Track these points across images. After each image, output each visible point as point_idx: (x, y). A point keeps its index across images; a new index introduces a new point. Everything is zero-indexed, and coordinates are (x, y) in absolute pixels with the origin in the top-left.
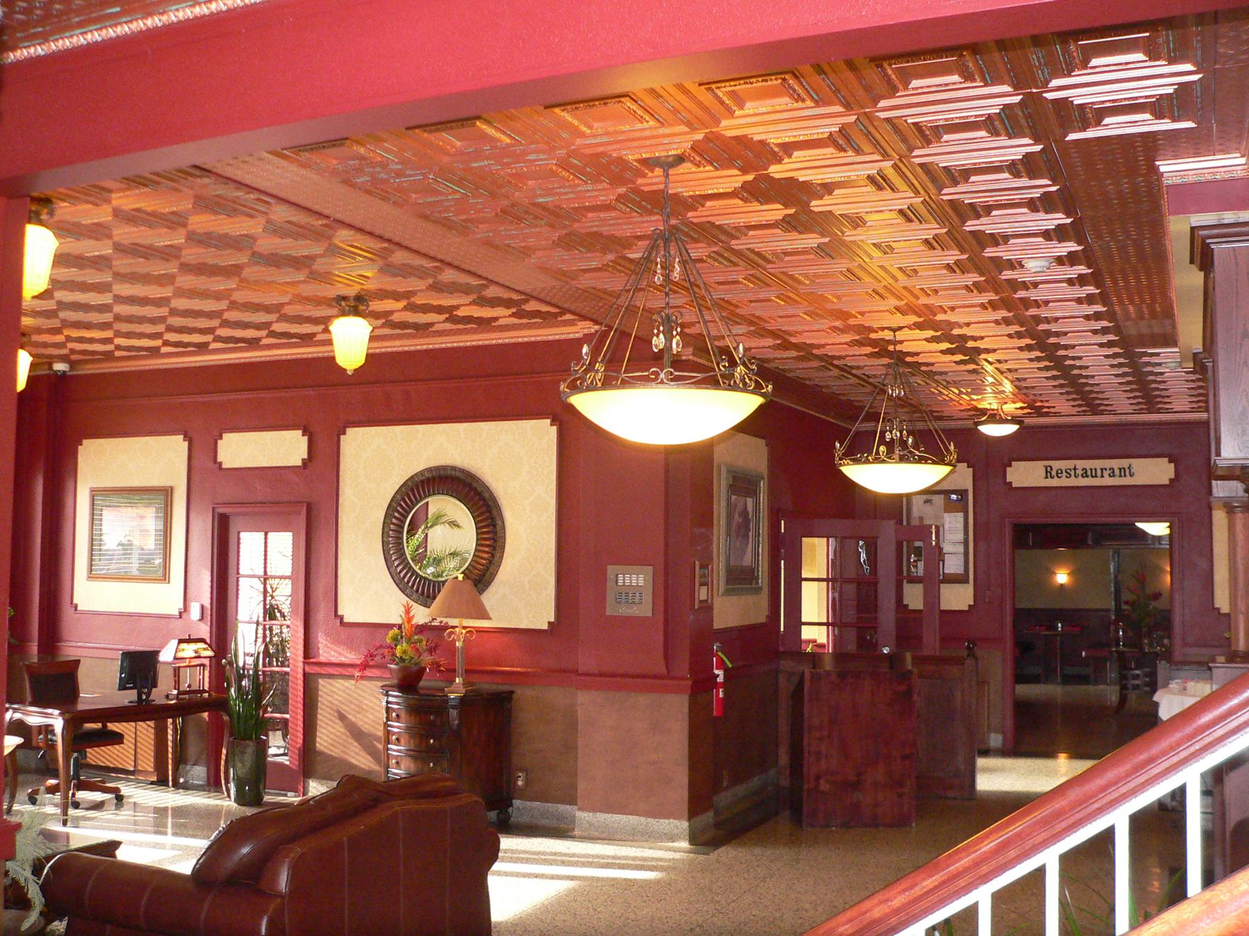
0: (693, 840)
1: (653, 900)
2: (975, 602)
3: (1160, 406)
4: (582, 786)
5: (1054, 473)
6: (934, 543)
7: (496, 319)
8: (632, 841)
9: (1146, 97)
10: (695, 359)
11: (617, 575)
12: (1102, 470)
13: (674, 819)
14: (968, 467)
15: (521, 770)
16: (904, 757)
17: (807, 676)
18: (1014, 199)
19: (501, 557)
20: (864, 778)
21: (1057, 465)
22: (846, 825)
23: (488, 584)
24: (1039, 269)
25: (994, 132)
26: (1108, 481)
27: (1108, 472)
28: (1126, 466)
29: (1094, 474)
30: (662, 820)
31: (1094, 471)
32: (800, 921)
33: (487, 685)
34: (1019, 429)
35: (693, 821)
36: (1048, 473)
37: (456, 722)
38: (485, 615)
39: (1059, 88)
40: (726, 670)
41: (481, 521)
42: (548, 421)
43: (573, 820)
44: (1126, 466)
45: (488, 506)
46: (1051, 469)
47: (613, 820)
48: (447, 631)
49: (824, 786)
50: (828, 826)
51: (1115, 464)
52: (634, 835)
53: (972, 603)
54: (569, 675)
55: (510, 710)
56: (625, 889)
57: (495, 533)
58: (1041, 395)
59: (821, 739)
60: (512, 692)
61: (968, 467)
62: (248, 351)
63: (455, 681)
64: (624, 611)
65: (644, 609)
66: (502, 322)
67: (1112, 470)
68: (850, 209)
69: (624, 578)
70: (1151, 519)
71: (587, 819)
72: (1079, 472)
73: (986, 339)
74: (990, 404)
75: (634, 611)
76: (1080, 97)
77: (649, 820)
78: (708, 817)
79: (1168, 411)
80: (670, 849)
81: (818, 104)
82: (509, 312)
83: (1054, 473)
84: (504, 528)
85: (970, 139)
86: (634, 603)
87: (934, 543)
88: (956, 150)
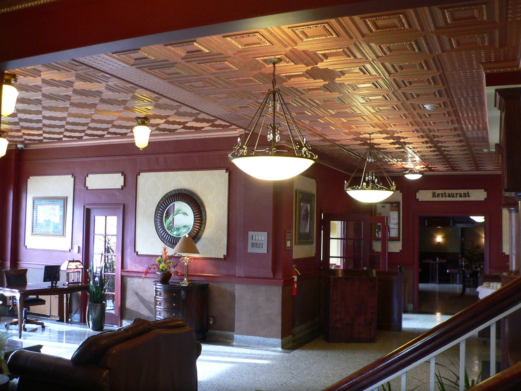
0: (284, 347)
5: (436, 195)
7: (203, 127)
11: (252, 236)
13: (275, 338)
15: (212, 317)
19: (204, 228)
21: (437, 192)
23: (199, 238)
26: (459, 199)
27: (459, 195)
29: (453, 196)
30: (270, 339)
31: (453, 195)
36: (434, 195)
40: (298, 277)
42: (225, 171)
46: (435, 194)
51: (462, 191)
54: (231, 277)
56: (254, 368)
63: (184, 279)
71: (239, 338)
72: (447, 195)
74: (410, 166)
77: (265, 338)
82: (209, 124)
83: (436, 195)
86: (259, 247)
87: (386, 224)
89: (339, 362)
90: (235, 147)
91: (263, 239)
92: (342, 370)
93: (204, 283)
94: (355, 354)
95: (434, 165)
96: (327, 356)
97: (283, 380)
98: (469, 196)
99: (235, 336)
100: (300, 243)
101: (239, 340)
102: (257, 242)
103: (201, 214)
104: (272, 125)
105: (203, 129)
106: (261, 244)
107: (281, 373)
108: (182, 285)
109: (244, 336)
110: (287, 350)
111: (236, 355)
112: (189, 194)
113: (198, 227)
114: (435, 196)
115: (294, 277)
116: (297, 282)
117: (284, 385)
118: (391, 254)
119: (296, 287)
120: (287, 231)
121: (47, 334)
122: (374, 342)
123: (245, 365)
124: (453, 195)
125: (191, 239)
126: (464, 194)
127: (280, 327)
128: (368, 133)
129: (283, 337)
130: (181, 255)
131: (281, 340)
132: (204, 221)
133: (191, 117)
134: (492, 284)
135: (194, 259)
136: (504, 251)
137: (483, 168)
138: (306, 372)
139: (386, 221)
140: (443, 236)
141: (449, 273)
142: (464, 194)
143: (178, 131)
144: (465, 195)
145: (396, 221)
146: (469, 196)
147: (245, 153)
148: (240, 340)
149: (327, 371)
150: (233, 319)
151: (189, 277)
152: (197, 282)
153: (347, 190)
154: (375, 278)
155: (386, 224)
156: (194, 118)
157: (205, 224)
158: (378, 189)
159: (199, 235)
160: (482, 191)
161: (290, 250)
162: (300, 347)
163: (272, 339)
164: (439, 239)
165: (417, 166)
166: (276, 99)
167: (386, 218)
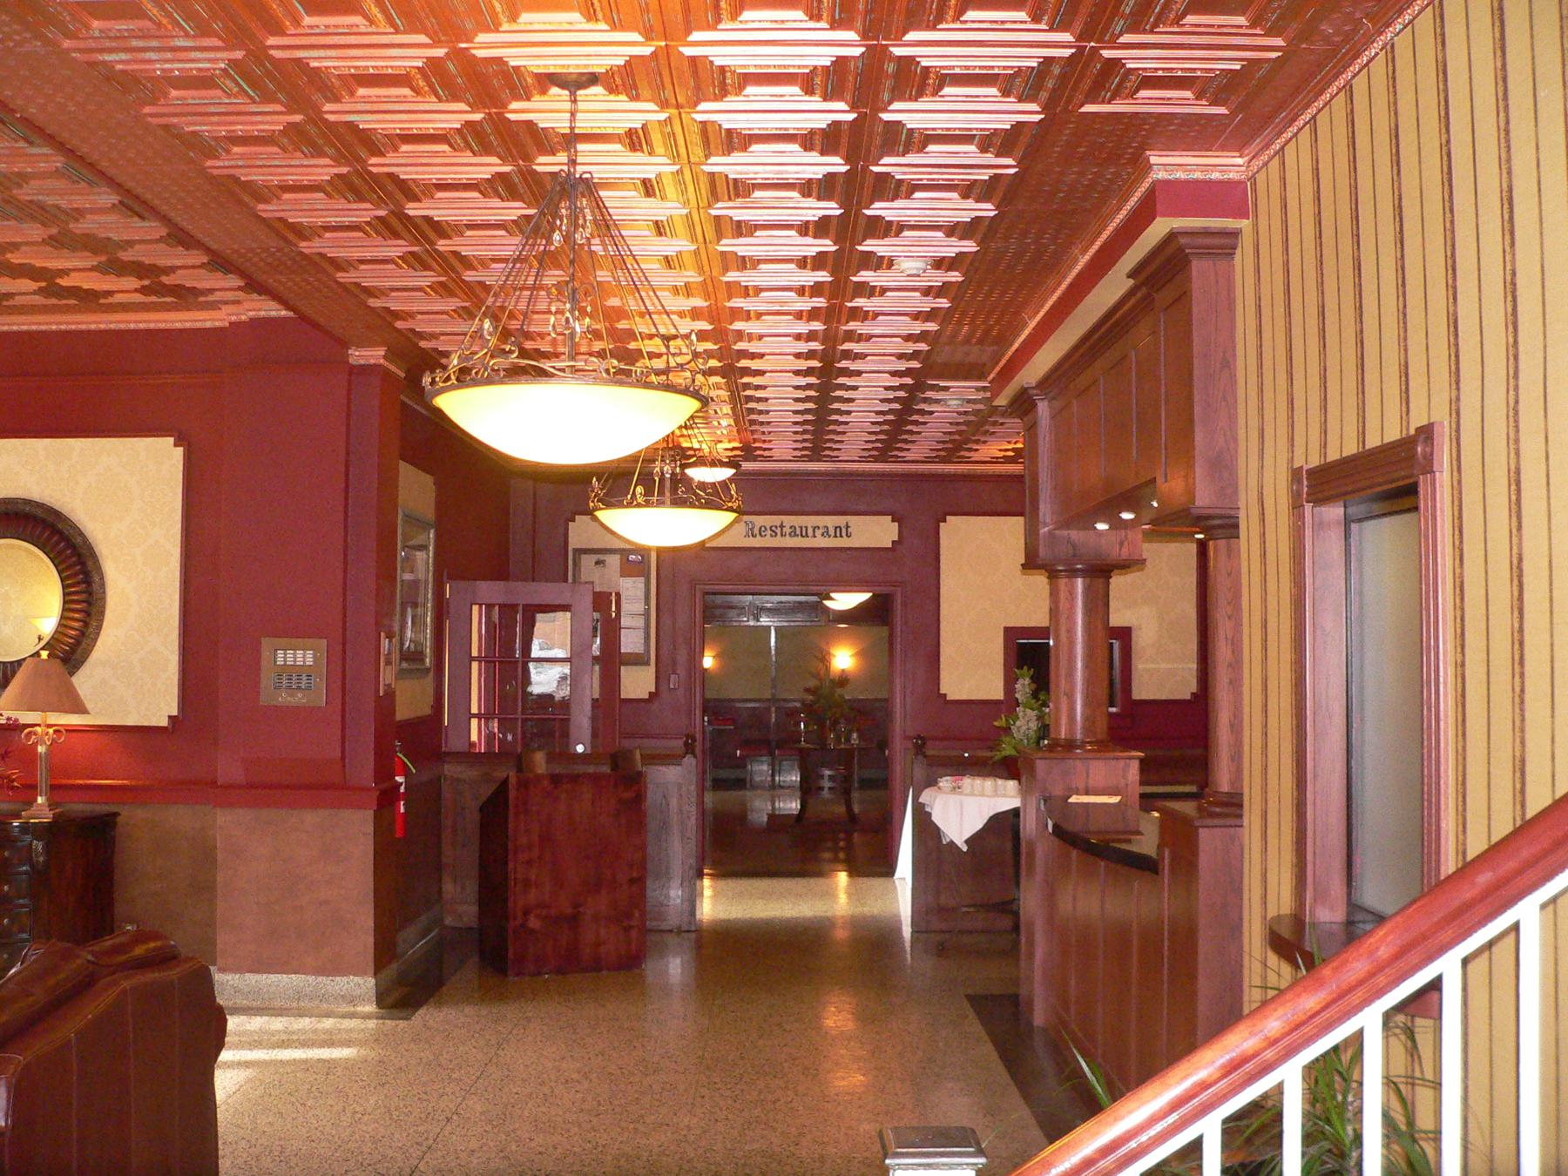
0: (381, 1000)
2: (656, 688)
3: (758, 452)
5: (756, 531)
6: (614, 614)
7: (110, 293)
9: (799, 67)
10: (386, 364)
13: (355, 975)
14: (893, 521)
16: (632, 881)
17: (513, 781)
18: (953, 180)
19: (99, 627)
20: (581, 909)
22: (560, 971)
24: (915, 272)
25: (809, 90)
27: (821, 531)
28: (843, 525)
29: (804, 534)
30: (338, 978)
31: (804, 530)
32: (579, 1096)
33: (79, 807)
34: (734, 475)
35: (379, 975)
37: (41, 859)
38: (80, 709)
39: (702, 44)
41: (68, 577)
44: (843, 525)
45: (79, 555)
47: (269, 982)
48: (26, 731)
49: (534, 923)
50: (539, 974)
51: (831, 521)
52: (299, 999)
55: (113, 838)
56: (328, 1074)
57: (90, 594)
58: (770, 433)
59: (529, 862)
60: (116, 815)
61: (893, 521)
62: (80, 311)
63: (36, 800)
64: (284, 698)
65: (316, 695)
68: (411, 173)
69: (285, 654)
70: (848, 588)
71: (231, 983)
72: (787, 530)
76: (721, 57)
77: (320, 979)
78: (392, 970)
79: (769, 459)
81: (614, 27)
83: (756, 531)
84: (103, 585)
85: (972, 96)
87: (614, 614)
88: (401, 109)
94: (603, 1006)
96: (529, 1020)
97: (442, 1105)
103: (88, 581)
105: (110, 300)
108: (32, 821)
109: (247, 975)
117: (455, 1117)
119: (402, 810)
124: (804, 530)
125: (57, 665)
130: (16, 720)
135: (67, 731)
137: (900, 454)
143: (18, 300)
145: (640, 607)
157: (102, 613)
158: (702, 507)
159: (79, 651)
162: (432, 995)
163: (345, 979)
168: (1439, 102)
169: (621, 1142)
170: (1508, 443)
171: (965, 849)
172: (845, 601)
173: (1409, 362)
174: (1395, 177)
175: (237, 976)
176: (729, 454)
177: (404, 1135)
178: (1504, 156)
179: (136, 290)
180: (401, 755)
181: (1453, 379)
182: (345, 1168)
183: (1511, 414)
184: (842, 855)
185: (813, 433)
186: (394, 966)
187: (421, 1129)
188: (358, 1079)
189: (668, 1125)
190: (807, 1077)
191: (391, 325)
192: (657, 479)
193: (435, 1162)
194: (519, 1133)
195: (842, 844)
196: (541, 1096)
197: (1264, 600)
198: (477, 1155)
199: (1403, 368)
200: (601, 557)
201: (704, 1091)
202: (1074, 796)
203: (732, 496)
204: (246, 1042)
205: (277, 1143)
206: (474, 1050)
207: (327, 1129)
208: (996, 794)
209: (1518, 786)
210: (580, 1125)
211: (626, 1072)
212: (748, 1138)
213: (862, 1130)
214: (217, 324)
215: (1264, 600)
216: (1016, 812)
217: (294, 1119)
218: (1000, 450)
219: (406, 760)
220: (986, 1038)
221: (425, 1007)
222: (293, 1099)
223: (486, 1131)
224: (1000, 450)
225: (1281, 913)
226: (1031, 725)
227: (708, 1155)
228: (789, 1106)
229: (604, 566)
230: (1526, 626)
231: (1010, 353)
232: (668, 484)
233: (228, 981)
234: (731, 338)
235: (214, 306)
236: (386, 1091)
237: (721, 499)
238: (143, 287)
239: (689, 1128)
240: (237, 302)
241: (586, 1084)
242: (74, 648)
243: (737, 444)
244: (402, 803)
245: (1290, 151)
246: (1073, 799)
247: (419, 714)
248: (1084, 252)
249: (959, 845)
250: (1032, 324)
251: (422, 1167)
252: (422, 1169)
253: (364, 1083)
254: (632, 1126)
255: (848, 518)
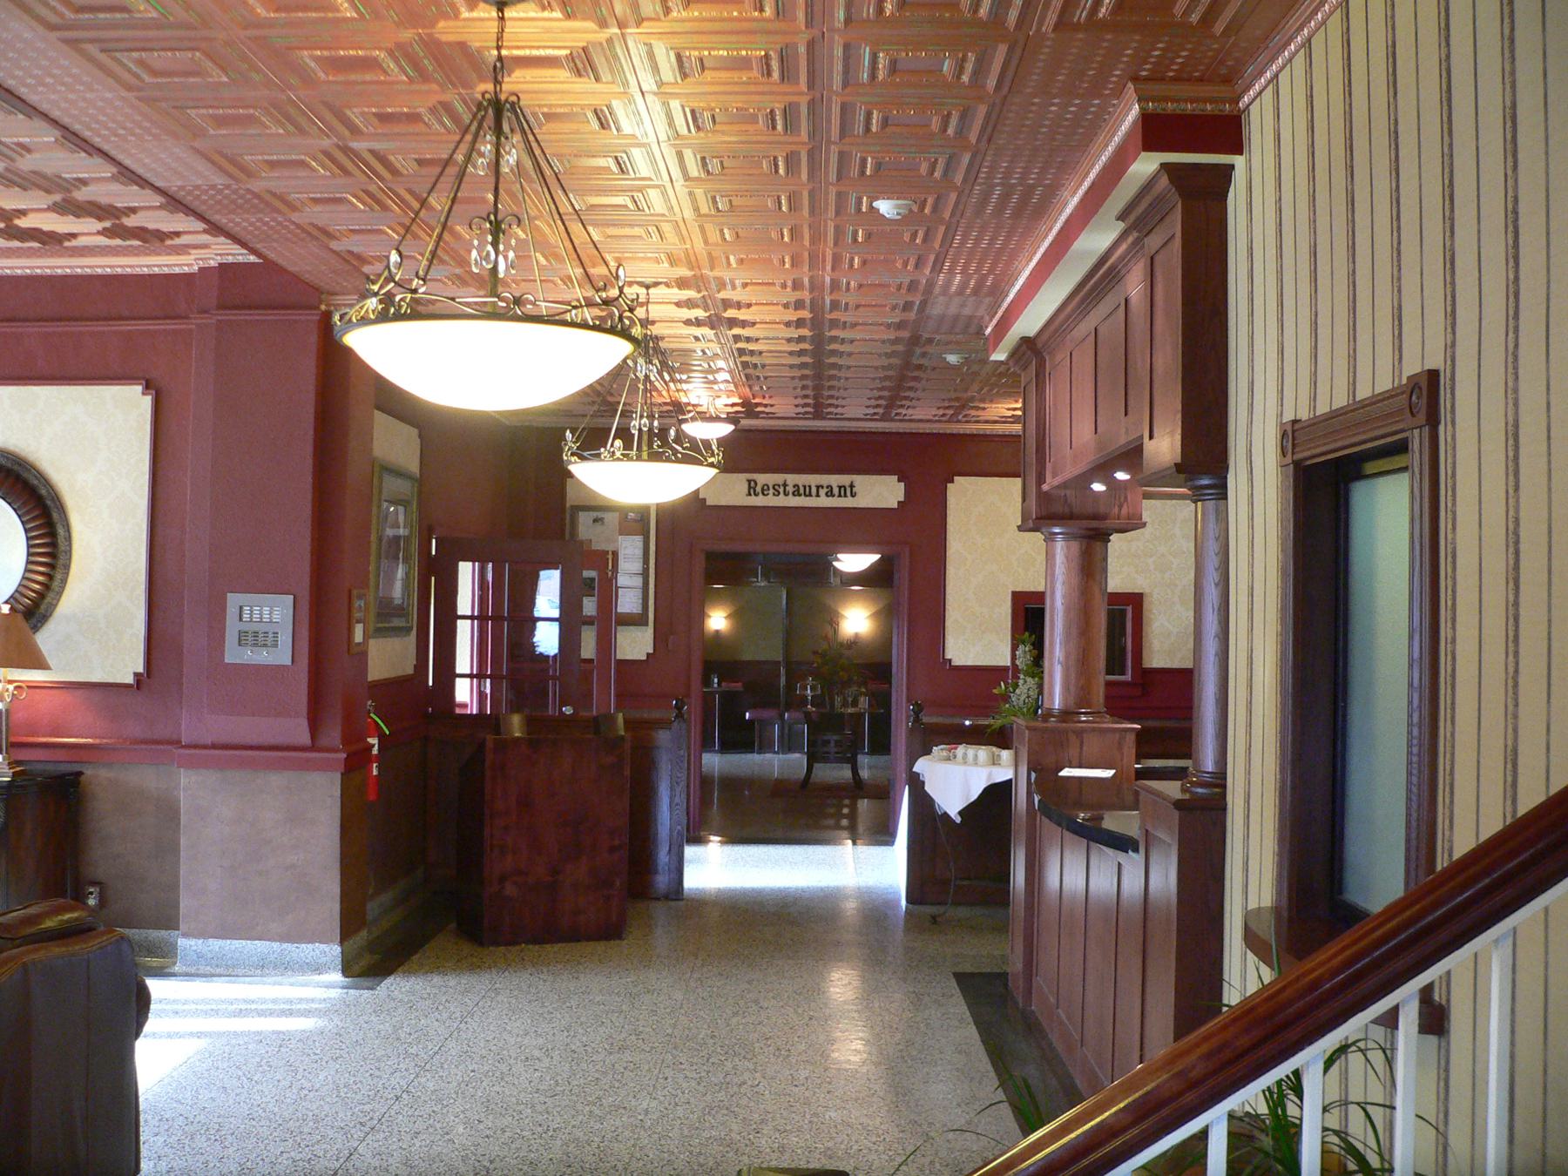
0: (347, 970)
1: (325, 1059)
3: (759, 409)
4: (185, 903)
5: (758, 489)
7: (74, 236)
8: (261, 976)
11: (241, 608)
12: (818, 487)
13: (320, 942)
15: (94, 883)
17: (490, 744)
19: (64, 581)
21: (762, 479)
23: (45, 618)
26: (824, 501)
27: (825, 490)
28: (847, 484)
29: (843, 489)
32: (537, 1074)
36: (752, 489)
40: (381, 736)
41: (32, 529)
42: (139, 388)
43: (174, 946)
44: (847, 484)
46: (756, 484)
49: (510, 890)
51: (835, 480)
53: (651, 651)
54: (166, 747)
56: (281, 1046)
60: (80, 774)
64: (249, 656)
66: (82, 241)
67: (830, 487)
72: (790, 489)
73: (754, 308)
74: (699, 397)
75: (264, 657)
77: (285, 945)
78: (362, 937)
80: (318, 985)
82: (99, 226)
86: (265, 645)
87: (610, 573)
89: (543, 1006)
90: (374, 283)
91: (276, 617)
92: (566, 1034)
93: (64, 768)
95: (770, 397)
96: (497, 993)
97: (393, 1082)
98: (853, 495)
99: (182, 942)
100: (381, 632)
101: (195, 957)
102: (257, 629)
103: (52, 534)
104: (492, 217)
105: (74, 243)
106: (271, 635)
107: (379, 1060)
110: (362, 979)
111: (199, 1007)
112: (9, 465)
113: (40, 578)
114: (755, 491)
115: (370, 740)
116: (378, 758)
117: (404, 1096)
118: (624, 664)
119: (375, 772)
120: (355, 592)
121: (329, 986)
122: (620, 938)
123: (246, 1039)
126: (840, 487)
127: (335, 907)
128: (641, 284)
129: (345, 936)
131: (339, 949)
132: (62, 557)
133: (48, 191)
134: (961, 750)
135: (28, 687)
136: (948, 656)
138: (453, 1047)
139: (610, 564)
140: (729, 612)
141: (751, 721)
142: (840, 487)
144: (843, 491)
145: (637, 566)
146: (853, 495)
147: (373, 311)
148: (200, 956)
149: (519, 1039)
150: (174, 887)
151: (12, 750)
152: (40, 767)
153: (570, 462)
154: (622, 738)
155: (610, 573)
156: (58, 197)
157: (67, 567)
158: (678, 461)
159: (43, 607)
160: (892, 479)
161: (362, 656)
164: (718, 620)
165: (719, 397)
166: (506, 127)
167: (610, 557)
168: (1439, 13)
169: (574, 1126)
170: (1506, 391)
171: (958, 820)
172: (853, 562)
173: (1403, 304)
174: (1391, 100)
175: (201, 941)
176: (730, 409)
177: (349, 1114)
178: (1508, 68)
179: (99, 233)
180: (374, 717)
181: (1449, 322)
182: (282, 1149)
183: (1510, 359)
184: (845, 822)
185: (822, 387)
186: (364, 933)
187: (367, 1108)
188: (310, 1052)
189: (624, 1108)
190: (778, 1057)
191: (357, 269)
192: (636, 433)
193: (376, 1145)
194: (468, 1114)
195: (846, 811)
196: (498, 1074)
197: (1251, 565)
198: (421, 1137)
199: (1396, 311)
200: (600, 515)
201: (668, 1072)
202: (1067, 769)
203: (713, 452)
204: (202, 1010)
205: (215, 1120)
206: (436, 1023)
207: (270, 1105)
208: (995, 761)
209: (1509, 779)
210: (533, 1106)
211: (590, 1050)
212: (707, 1124)
213: (827, 1117)
214: (186, 269)
215: (1251, 565)
216: (1007, 785)
217: (237, 1095)
218: (1009, 409)
219: (377, 719)
220: (970, 1020)
221: (392, 977)
222: (240, 1073)
223: (434, 1111)
224: (1009, 409)
225: (1262, 905)
226: (1031, 693)
227: (663, 1142)
228: (755, 1090)
229: (603, 524)
230: (1522, 599)
231: (1005, 305)
232: (645, 437)
233: (191, 946)
234: (713, 286)
235: (183, 250)
236: (338, 1066)
237: (702, 455)
238: (104, 229)
239: (647, 1112)
240: (206, 246)
241: (546, 1061)
242: (36, 604)
243: (737, 400)
244: (375, 765)
245: (1284, 78)
246: (1066, 772)
247: (400, 673)
248: (1073, 195)
249: (953, 816)
250: (1026, 273)
251: (360, 1149)
252: (361, 1152)
253: (317, 1057)
254: (587, 1108)
255: (854, 477)
